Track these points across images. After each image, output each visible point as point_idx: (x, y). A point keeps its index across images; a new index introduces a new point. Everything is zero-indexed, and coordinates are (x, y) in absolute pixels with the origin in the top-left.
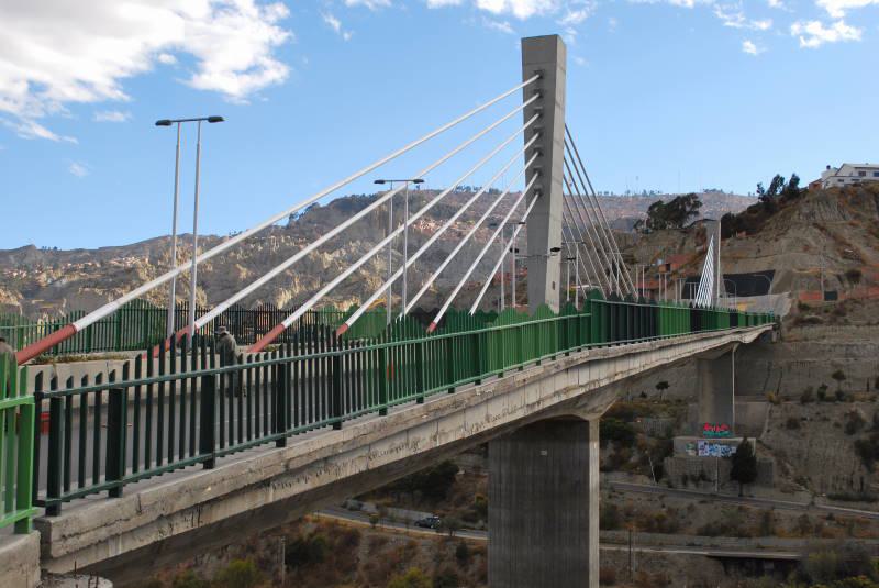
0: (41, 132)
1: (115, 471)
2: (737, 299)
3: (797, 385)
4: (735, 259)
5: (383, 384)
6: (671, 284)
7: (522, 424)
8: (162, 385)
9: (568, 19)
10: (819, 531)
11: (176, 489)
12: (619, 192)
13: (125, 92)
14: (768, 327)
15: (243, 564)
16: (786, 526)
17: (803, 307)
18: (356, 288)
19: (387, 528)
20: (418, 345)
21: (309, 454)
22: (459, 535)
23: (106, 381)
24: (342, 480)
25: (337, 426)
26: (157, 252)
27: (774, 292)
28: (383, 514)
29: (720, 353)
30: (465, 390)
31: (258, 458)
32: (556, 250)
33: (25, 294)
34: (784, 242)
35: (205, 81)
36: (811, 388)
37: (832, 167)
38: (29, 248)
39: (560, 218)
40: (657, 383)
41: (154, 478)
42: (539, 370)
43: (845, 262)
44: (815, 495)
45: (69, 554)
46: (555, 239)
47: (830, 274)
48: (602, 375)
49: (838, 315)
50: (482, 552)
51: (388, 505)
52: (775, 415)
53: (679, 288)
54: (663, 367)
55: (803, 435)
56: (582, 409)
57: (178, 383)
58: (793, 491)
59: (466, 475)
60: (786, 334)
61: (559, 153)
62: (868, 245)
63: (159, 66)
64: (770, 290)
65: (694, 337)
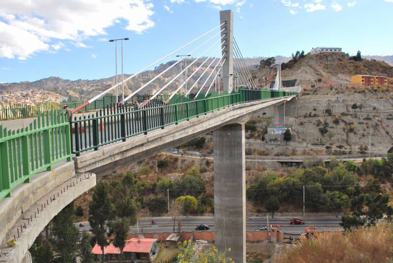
0: (82, 45)
1: (96, 143)
2: (285, 88)
3: (303, 112)
4: (285, 76)
5: (176, 116)
6: (266, 85)
7: (222, 126)
8: (108, 118)
9: (238, 5)
10: (308, 154)
11: (114, 148)
12: (251, 57)
13: (106, 32)
14: (295, 96)
15: (146, 168)
16: (299, 153)
17: (305, 90)
18: (173, 87)
19: (186, 157)
20: (187, 104)
21: (154, 136)
22: (206, 158)
23: (91, 117)
24: (166, 144)
25: (163, 128)
26: (117, 79)
28: (185, 153)
29: (280, 104)
30: (202, 116)
31: (140, 138)
32: (232, 75)
33: (80, 93)
34: (299, 71)
35: (129, 28)
36: (307, 114)
38: (80, 80)
39: (232, 65)
40: (263, 113)
41: (108, 144)
42: (224, 110)
43: (317, 76)
44: (308, 144)
45: (83, 167)
46: (231, 71)
47: (313, 80)
48: (244, 111)
49: (315, 92)
50: (212, 162)
51: (186, 150)
52: (296, 121)
53: (268, 86)
54: (263, 108)
55: (305, 127)
57: (103, 119)
58: (301, 143)
59: (208, 141)
60: (300, 98)
61: (232, 46)
62: (324, 71)
63: (115, 23)
64: (296, 84)
65: (272, 99)
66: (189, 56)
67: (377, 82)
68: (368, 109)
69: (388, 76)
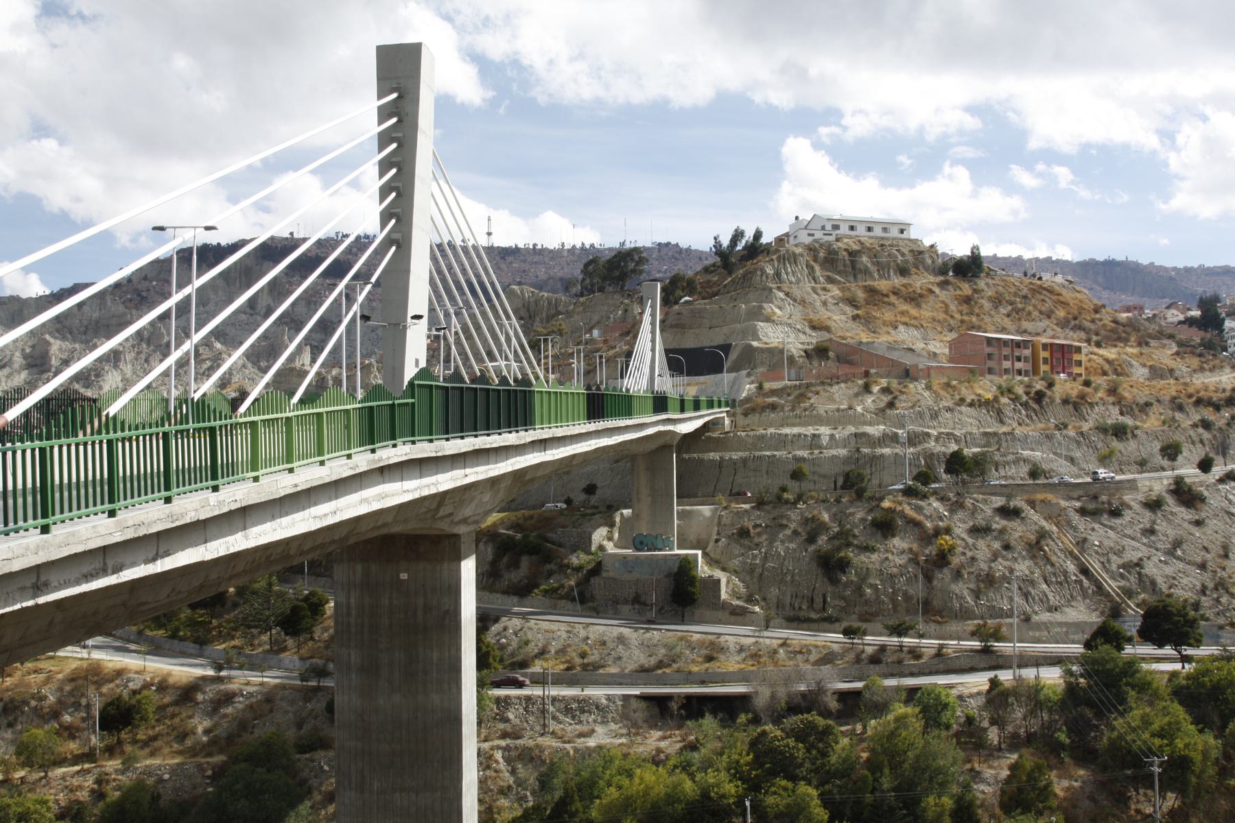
27: (730, 371)
29: (653, 446)
32: (418, 317)
37: (800, 218)
56: (448, 520)
65: (592, 426)
66: (208, 228)
67: (1045, 361)
68: (1012, 471)
69: (1088, 341)
